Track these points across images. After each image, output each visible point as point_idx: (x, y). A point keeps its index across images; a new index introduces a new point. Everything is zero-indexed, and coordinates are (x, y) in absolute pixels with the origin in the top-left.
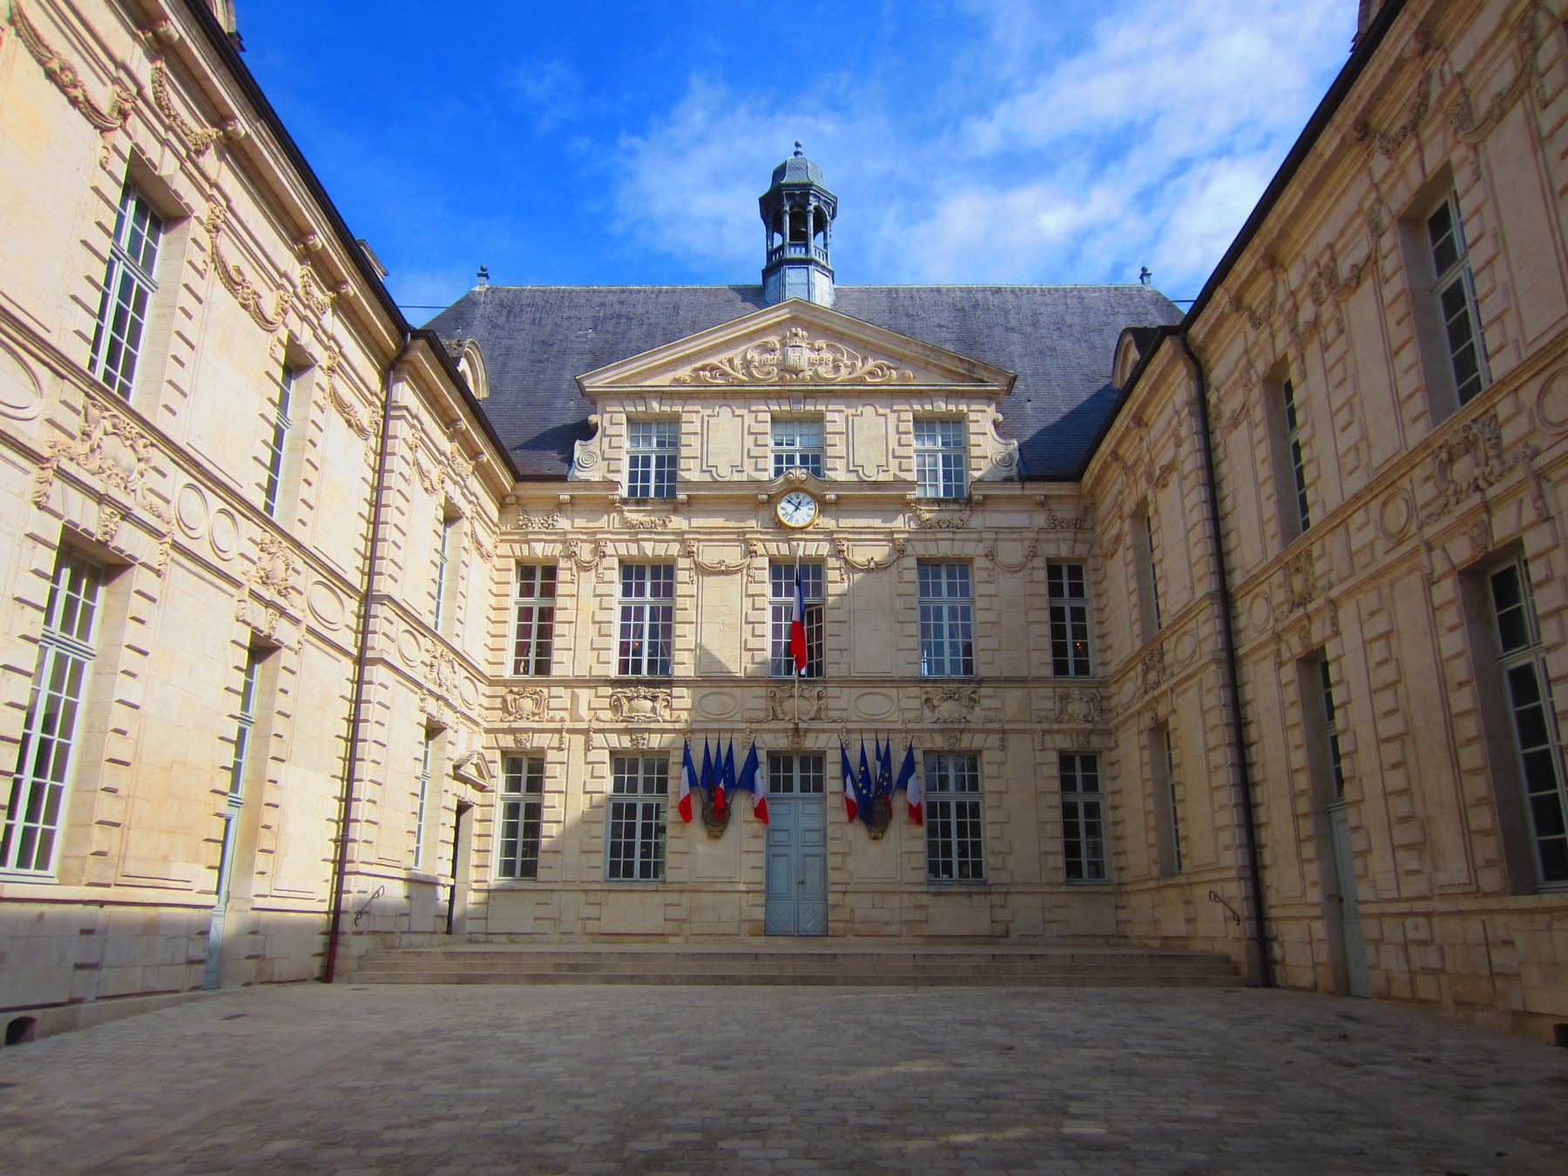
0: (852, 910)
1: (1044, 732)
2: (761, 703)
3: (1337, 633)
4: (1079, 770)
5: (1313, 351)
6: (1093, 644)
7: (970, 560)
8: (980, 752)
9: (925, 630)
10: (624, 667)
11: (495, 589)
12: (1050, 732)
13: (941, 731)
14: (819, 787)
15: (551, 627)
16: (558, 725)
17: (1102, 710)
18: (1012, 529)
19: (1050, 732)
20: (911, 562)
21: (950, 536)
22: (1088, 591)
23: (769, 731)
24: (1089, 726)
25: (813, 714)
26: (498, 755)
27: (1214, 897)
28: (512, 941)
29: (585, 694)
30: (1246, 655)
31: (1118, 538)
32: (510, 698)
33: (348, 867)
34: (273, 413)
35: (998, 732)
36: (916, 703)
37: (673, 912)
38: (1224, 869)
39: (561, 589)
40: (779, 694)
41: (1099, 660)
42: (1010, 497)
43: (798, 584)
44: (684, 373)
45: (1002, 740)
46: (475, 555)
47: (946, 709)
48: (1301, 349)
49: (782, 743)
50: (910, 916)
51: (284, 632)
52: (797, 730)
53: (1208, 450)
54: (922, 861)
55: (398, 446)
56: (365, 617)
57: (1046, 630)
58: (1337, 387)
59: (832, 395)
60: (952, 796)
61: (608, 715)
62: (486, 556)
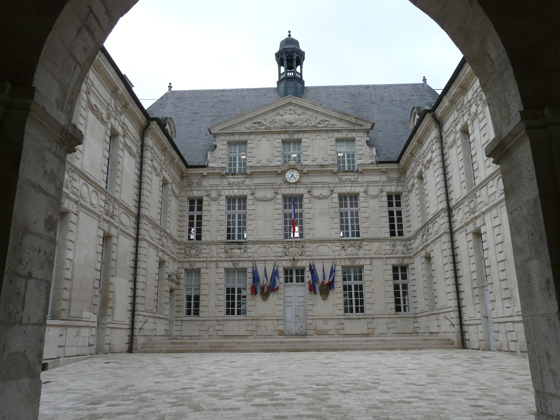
0: (316, 326)
1: (387, 258)
2: (281, 250)
3: (484, 224)
4: (400, 271)
5: (476, 122)
6: (405, 224)
7: (358, 194)
8: (363, 266)
9: (342, 221)
10: (229, 237)
11: (180, 208)
12: (389, 258)
13: (348, 259)
14: (303, 281)
15: (201, 222)
16: (205, 259)
17: (408, 249)
18: (374, 182)
19: (389, 258)
20: (336, 195)
21: (350, 185)
22: (403, 204)
23: (284, 260)
24: (403, 255)
25: (300, 254)
26: (183, 271)
27: (446, 318)
28: (191, 339)
29: (214, 247)
30: (456, 231)
31: (413, 185)
32: (187, 249)
33: (136, 313)
34: (107, 154)
35: (370, 258)
36: (339, 248)
37: (250, 328)
38: (449, 307)
39: (204, 208)
40: (287, 246)
41: (407, 231)
42: (373, 170)
43: (293, 204)
44: (249, 124)
45: (371, 261)
46: (173, 197)
47: (350, 250)
48: (473, 121)
49: (289, 264)
50: (338, 327)
51: (114, 231)
52: (294, 260)
53: (443, 155)
54: (342, 307)
55: (147, 161)
56: (138, 223)
57: (387, 219)
58: (483, 136)
59: (305, 132)
60: (353, 283)
61: (222, 255)
62: (177, 197)
